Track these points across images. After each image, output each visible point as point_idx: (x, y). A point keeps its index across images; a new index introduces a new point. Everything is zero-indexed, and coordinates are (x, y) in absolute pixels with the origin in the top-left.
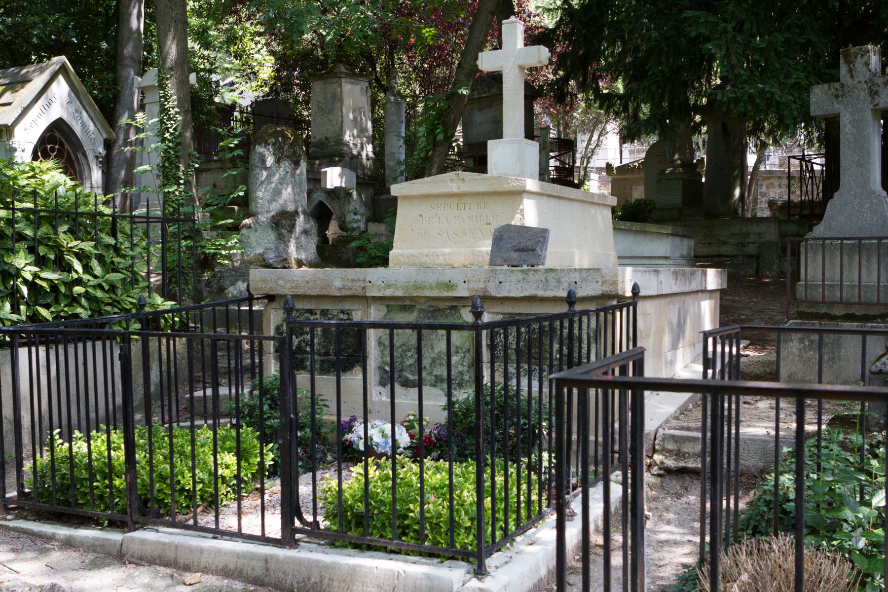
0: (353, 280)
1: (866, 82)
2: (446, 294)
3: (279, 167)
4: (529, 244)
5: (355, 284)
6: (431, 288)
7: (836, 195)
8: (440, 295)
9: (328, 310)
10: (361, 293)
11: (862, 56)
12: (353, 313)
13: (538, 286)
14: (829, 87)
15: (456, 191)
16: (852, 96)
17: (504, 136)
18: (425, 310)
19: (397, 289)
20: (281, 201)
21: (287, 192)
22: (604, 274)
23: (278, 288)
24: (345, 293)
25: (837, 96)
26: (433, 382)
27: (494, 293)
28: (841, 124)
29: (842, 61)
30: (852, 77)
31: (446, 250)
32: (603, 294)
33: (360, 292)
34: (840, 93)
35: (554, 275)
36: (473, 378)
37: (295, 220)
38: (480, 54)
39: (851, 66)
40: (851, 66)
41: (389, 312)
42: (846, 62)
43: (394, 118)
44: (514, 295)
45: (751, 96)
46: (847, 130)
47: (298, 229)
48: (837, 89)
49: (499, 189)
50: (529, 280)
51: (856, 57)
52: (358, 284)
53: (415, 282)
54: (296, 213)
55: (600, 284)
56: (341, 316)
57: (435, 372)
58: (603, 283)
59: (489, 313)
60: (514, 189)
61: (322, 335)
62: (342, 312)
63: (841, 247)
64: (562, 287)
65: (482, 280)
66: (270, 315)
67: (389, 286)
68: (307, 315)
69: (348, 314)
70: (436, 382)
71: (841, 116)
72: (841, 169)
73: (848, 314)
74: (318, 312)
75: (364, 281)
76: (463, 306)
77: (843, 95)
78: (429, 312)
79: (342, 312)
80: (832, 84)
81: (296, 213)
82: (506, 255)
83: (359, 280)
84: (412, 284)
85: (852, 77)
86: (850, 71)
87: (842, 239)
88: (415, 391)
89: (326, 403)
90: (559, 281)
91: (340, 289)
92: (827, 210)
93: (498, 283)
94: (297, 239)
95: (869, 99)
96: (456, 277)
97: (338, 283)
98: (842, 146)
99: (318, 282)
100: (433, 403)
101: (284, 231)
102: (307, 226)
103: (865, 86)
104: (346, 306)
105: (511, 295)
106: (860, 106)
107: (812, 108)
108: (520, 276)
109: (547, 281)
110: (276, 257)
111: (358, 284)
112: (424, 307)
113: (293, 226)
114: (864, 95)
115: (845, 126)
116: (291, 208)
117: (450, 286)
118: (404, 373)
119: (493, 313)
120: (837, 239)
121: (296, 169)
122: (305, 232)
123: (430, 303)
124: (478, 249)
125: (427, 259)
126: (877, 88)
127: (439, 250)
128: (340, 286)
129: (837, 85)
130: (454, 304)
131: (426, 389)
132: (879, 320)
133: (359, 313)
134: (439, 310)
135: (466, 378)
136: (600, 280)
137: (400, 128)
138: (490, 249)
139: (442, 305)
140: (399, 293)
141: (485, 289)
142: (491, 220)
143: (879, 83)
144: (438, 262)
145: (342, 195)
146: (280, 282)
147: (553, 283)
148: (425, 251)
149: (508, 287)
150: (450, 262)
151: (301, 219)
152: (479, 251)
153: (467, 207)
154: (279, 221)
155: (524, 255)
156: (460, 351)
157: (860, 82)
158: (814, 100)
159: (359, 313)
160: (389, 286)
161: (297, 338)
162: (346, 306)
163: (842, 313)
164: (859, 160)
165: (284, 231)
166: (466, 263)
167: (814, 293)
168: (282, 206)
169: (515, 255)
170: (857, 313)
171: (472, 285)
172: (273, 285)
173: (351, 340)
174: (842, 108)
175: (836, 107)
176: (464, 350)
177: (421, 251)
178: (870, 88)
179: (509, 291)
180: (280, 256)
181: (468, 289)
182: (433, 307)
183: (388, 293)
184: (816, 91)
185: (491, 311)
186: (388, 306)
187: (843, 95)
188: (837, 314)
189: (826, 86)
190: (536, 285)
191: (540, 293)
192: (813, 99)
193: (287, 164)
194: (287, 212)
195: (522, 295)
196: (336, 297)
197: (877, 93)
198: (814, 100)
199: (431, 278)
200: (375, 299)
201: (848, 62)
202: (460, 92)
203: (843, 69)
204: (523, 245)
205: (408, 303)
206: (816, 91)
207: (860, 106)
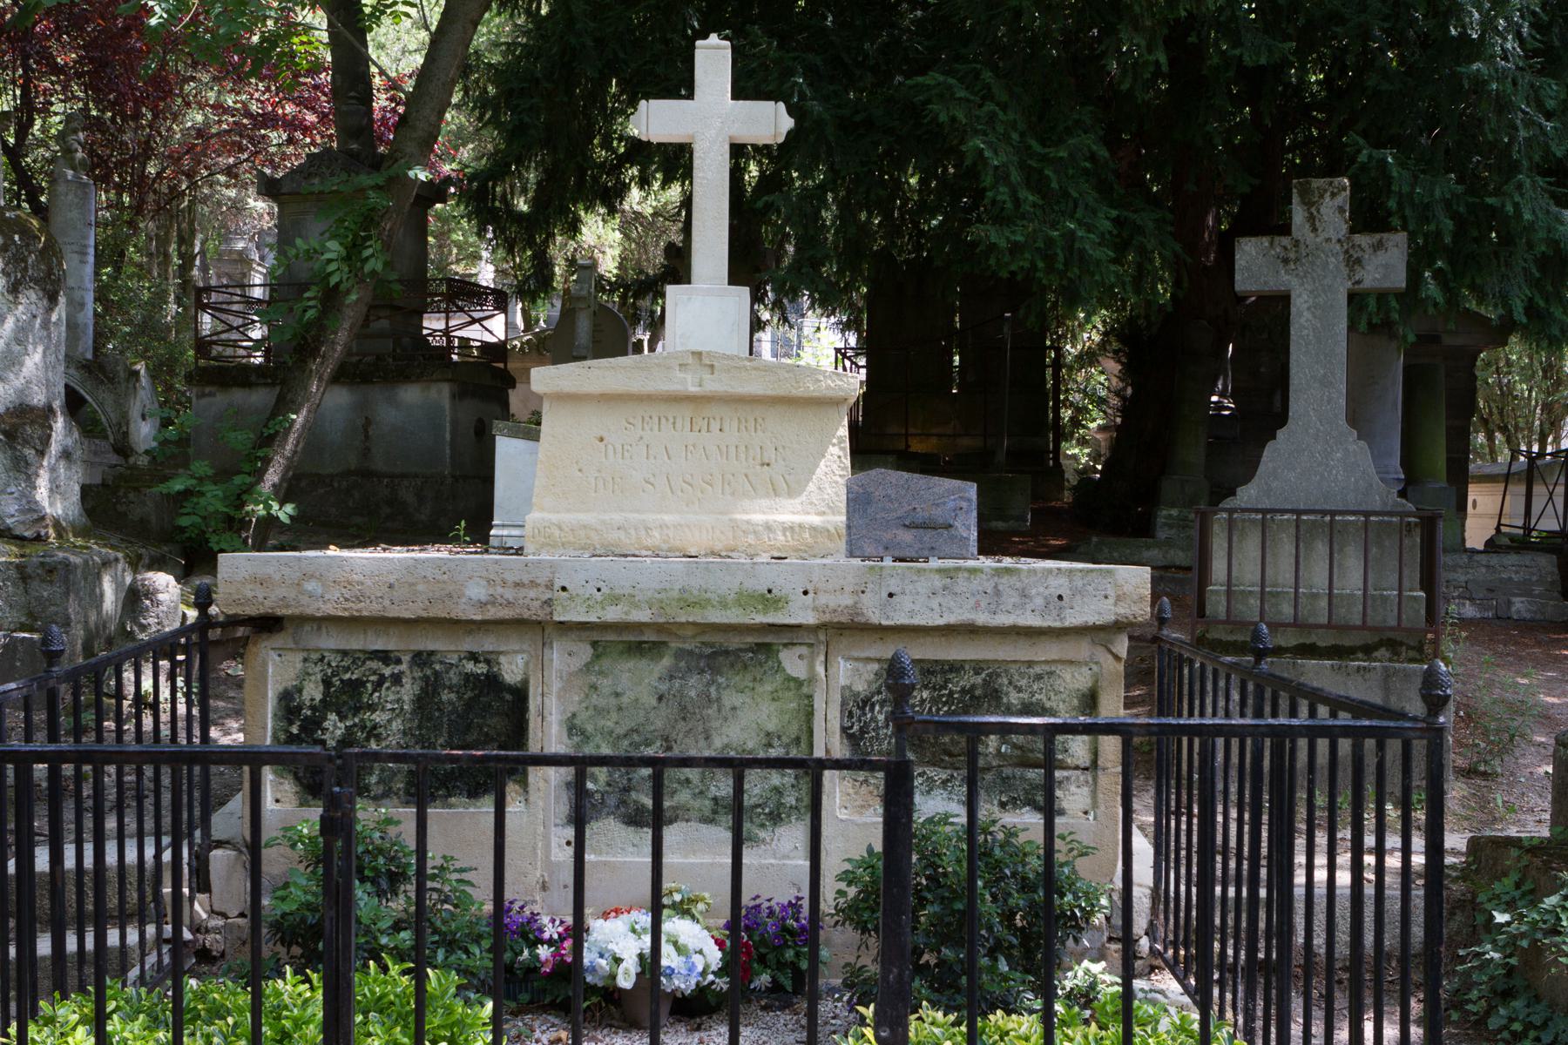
0: (517, 585)
1: (1339, 241)
2: (760, 619)
3: (16, 303)
4: (938, 514)
5: (523, 592)
6: (724, 605)
7: (1281, 434)
8: (747, 620)
9: (432, 653)
10: (542, 615)
11: (1333, 195)
12: (502, 659)
13: (978, 604)
14: (1272, 243)
15: (693, 389)
16: (1313, 263)
17: (694, 277)
18: (691, 653)
19: (636, 606)
20: (18, 383)
21: (34, 360)
22: (1121, 582)
23: (305, 600)
24: (493, 613)
25: (1286, 261)
26: (707, 813)
27: (875, 617)
28: (1293, 310)
29: (1296, 199)
30: (1315, 230)
31: (667, 518)
32: (1116, 622)
33: (535, 612)
34: (1292, 255)
35: (1013, 580)
36: (807, 800)
37: (51, 428)
38: (643, 102)
39: (1313, 210)
40: (1313, 210)
41: (597, 656)
42: (1304, 203)
43: (74, 214)
44: (923, 623)
45: (1050, 242)
46: (1302, 320)
47: (54, 448)
48: (1285, 248)
49: (794, 392)
50: (958, 589)
51: (1322, 196)
52: (532, 594)
53: (683, 590)
54: (48, 411)
55: (1111, 600)
56: (470, 666)
57: (713, 791)
58: (1118, 599)
59: (848, 659)
60: (830, 393)
61: (414, 712)
62: (473, 657)
63: (1297, 527)
64: (1029, 607)
65: (848, 589)
66: (265, 665)
67: (615, 599)
68: (374, 665)
69: (488, 662)
70: (715, 812)
71: (1293, 296)
72: (1291, 388)
73: (1303, 645)
74: (406, 658)
75: (550, 586)
76: (785, 645)
77: (1297, 260)
78: (701, 656)
79: (473, 657)
80: (1277, 239)
81: (48, 411)
82: (887, 536)
83: (533, 584)
84: (675, 594)
85: (1315, 230)
86: (1311, 219)
87: (1299, 512)
88: (647, 834)
89: (465, 876)
90: (1024, 595)
91: (482, 605)
92: (1264, 459)
93: (885, 595)
94: (53, 470)
95: (1345, 271)
96: (786, 581)
97: (477, 591)
98: (1292, 348)
99: (420, 587)
100: (718, 859)
101: (29, 453)
102: (69, 442)
103: (1338, 247)
104: (487, 644)
105: (917, 621)
106: (1327, 281)
107: (1238, 277)
108: (938, 582)
109: (997, 593)
110: (22, 511)
111: (532, 594)
112: (687, 646)
113: (46, 440)
114: (1335, 262)
115: (1300, 315)
116: (38, 398)
117: (769, 599)
118: (634, 795)
119: (857, 659)
120: (1257, 511)
121: (50, 310)
122: (66, 455)
123: (706, 638)
124: (745, 517)
125: (622, 535)
126: (1360, 254)
127: (650, 517)
128: (483, 599)
129: (1285, 241)
130: (768, 640)
131: (670, 834)
132: (1360, 655)
133: (520, 660)
134: (727, 653)
135: (790, 800)
136: (1111, 593)
137: (86, 237)
138: (842, 519)
139: (734, 642)
140: (642, 616)
141: (855, 609)
142: (770, 455)
143: (1364, 245)
144: (649, 542)
145: (122, 374)
146: (310, 586)
147: (1011, 599)
148: (617, 517)
149: (908, 606)
150: (678, 543)
151: (59, 424)
152: (748, 522)
153: (715, 426)
154: (15, 427)
155: (928, 536)
156: (776, 742)
157: (1328, 240)
158: (1243, 263)
159: (520, 660)
160: (615, 599)
161: (342, 718)
162: (487, 644)
163: (1293, 642)
164: (1325, 375)
165: (29, 453)
166: (718, 546)
167: (1240, 606)
168: (21, 392)
169: (906, 536)
170: (1321, 644)
171: (823, 599)
172: (291, 594)
173: (493, 721)
174: (1295, 282)
175: (1281, 280)
176: (785, 740)
177: (606, 517)
178: (1347, 252)
179: (912, 613)
180: (31, 510)
181: (815, 609)
182: (712, 645)
183: (612, 614)
184: (1247, 248)
185: (856, 654)
186: (594, 644)
187: (1297, 260)
188: (1283, 644)
189: (1265, 241)
190: (972, 601)
191: (982, 619)
192: (1241, 260)
193: (33, 297)
194: (32, 409)
195: (941, 622)
196: (472, 622)
197: (1358, 261)
198: (1243, 263)
199: (726, 585)
200: (565, 628)
201: (1308, 204)
202: (411, 174)
203: (1298, 215)
204: (921, 515)
205: (650, 636)
206: (1247, 248)
207: (1327, 281)
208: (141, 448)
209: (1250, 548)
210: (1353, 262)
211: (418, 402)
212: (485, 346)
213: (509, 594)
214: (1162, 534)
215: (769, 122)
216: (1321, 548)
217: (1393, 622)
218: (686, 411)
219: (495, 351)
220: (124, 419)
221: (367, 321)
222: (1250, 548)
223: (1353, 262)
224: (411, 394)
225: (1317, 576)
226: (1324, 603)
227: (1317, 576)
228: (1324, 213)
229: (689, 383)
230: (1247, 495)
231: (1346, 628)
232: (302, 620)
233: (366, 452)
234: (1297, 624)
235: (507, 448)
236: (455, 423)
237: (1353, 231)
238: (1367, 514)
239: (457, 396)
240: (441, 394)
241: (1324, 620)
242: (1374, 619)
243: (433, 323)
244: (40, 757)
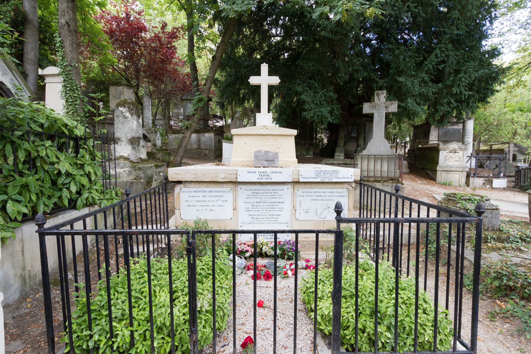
5: (231, 176)
10: (235, 181)
33: (234, 180)
99: (211, 175)
111: (233, 176)
153: (268, 141)
203: (376, 98)
208: (158, 145)
209: (365, 162)
210: (387, 107)
211: (209, 136)
212: (220, 126)
213: (229, 176)
214: (336, 158)
215: (275, 80)
216: (379, 162)
217: (393, 176)
218: (262, 137)
219: (222, 127)
220: (155, 140)
221: (199, 122)
222: (365, 162)
223: (387, 107)
224: (207, 135)
225: (378, 167)
226: (379, 172)
227: (378, 167)
228: (381, 97)
229: (263, 132)
230: (365, 152)
231: (384, 177)
232: (186, 182)
233: (199, 145)
234: (374, 177)
235: (226, 146)
236: (215, 140)
237: (386, 101)
238: (388, 156)
239: (215, 135)
240: (212, 135)
241: (379, 176)
242: (390, 176)
243: (210, 122)
244: (111, 233)
